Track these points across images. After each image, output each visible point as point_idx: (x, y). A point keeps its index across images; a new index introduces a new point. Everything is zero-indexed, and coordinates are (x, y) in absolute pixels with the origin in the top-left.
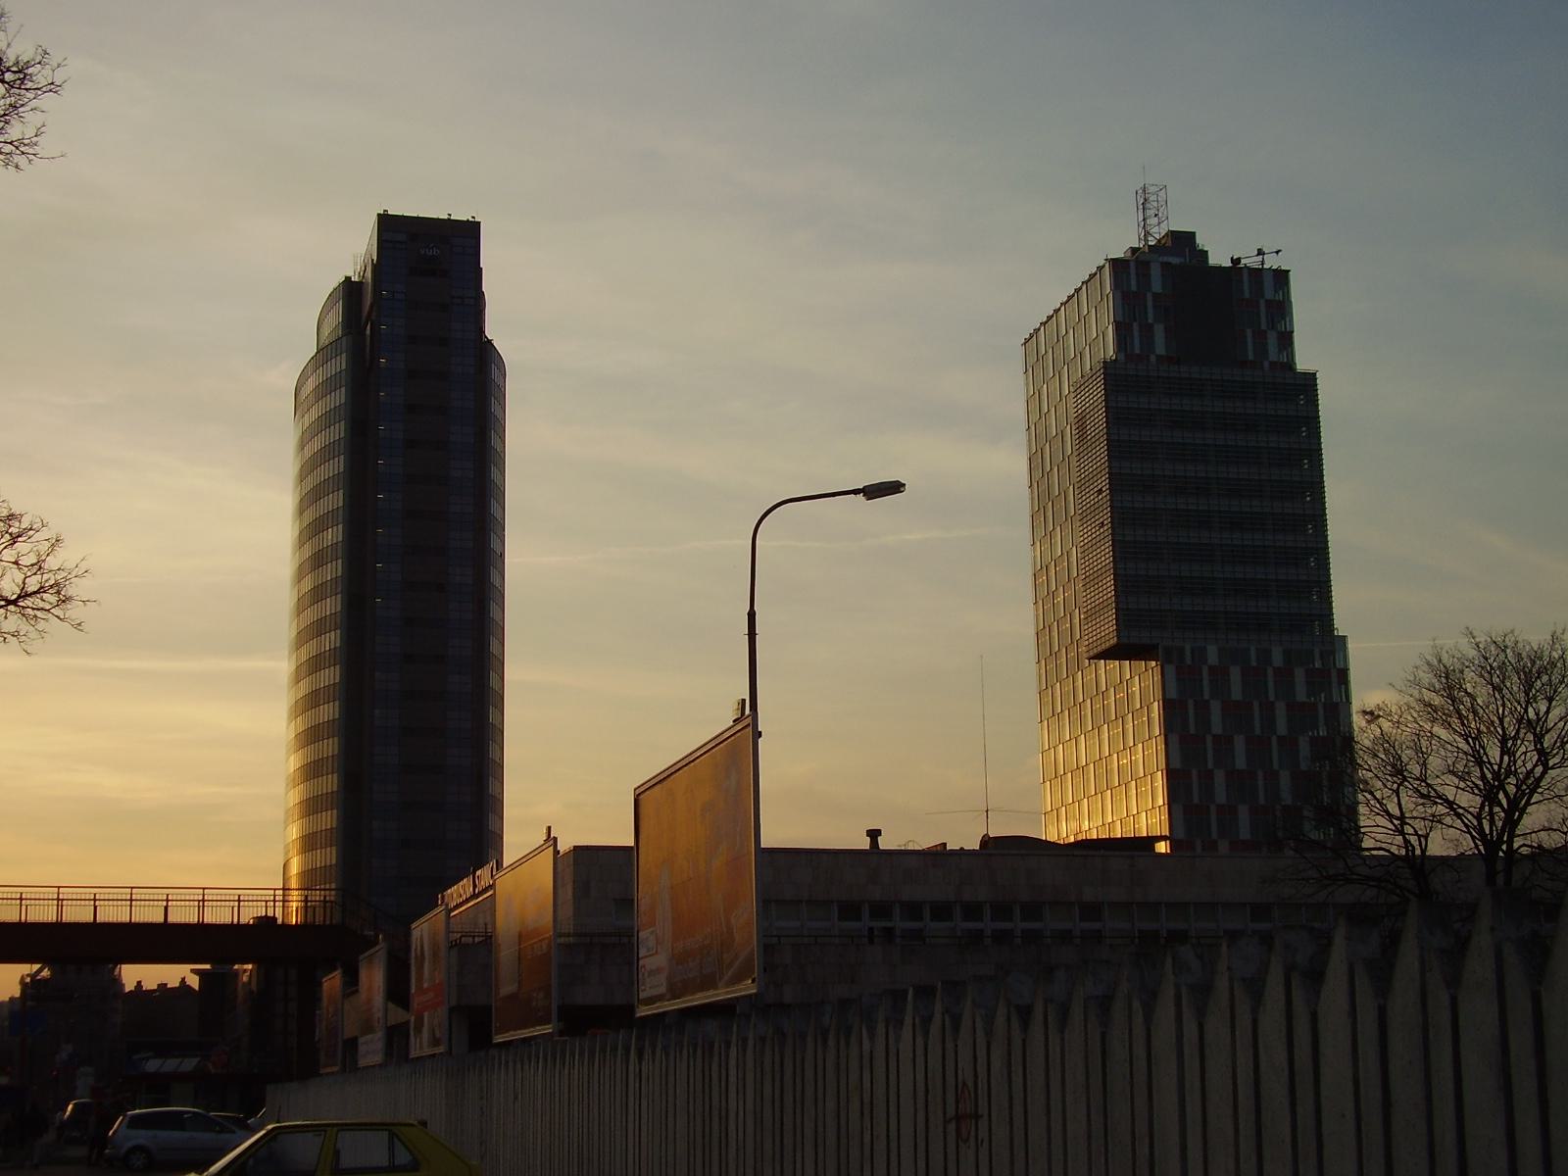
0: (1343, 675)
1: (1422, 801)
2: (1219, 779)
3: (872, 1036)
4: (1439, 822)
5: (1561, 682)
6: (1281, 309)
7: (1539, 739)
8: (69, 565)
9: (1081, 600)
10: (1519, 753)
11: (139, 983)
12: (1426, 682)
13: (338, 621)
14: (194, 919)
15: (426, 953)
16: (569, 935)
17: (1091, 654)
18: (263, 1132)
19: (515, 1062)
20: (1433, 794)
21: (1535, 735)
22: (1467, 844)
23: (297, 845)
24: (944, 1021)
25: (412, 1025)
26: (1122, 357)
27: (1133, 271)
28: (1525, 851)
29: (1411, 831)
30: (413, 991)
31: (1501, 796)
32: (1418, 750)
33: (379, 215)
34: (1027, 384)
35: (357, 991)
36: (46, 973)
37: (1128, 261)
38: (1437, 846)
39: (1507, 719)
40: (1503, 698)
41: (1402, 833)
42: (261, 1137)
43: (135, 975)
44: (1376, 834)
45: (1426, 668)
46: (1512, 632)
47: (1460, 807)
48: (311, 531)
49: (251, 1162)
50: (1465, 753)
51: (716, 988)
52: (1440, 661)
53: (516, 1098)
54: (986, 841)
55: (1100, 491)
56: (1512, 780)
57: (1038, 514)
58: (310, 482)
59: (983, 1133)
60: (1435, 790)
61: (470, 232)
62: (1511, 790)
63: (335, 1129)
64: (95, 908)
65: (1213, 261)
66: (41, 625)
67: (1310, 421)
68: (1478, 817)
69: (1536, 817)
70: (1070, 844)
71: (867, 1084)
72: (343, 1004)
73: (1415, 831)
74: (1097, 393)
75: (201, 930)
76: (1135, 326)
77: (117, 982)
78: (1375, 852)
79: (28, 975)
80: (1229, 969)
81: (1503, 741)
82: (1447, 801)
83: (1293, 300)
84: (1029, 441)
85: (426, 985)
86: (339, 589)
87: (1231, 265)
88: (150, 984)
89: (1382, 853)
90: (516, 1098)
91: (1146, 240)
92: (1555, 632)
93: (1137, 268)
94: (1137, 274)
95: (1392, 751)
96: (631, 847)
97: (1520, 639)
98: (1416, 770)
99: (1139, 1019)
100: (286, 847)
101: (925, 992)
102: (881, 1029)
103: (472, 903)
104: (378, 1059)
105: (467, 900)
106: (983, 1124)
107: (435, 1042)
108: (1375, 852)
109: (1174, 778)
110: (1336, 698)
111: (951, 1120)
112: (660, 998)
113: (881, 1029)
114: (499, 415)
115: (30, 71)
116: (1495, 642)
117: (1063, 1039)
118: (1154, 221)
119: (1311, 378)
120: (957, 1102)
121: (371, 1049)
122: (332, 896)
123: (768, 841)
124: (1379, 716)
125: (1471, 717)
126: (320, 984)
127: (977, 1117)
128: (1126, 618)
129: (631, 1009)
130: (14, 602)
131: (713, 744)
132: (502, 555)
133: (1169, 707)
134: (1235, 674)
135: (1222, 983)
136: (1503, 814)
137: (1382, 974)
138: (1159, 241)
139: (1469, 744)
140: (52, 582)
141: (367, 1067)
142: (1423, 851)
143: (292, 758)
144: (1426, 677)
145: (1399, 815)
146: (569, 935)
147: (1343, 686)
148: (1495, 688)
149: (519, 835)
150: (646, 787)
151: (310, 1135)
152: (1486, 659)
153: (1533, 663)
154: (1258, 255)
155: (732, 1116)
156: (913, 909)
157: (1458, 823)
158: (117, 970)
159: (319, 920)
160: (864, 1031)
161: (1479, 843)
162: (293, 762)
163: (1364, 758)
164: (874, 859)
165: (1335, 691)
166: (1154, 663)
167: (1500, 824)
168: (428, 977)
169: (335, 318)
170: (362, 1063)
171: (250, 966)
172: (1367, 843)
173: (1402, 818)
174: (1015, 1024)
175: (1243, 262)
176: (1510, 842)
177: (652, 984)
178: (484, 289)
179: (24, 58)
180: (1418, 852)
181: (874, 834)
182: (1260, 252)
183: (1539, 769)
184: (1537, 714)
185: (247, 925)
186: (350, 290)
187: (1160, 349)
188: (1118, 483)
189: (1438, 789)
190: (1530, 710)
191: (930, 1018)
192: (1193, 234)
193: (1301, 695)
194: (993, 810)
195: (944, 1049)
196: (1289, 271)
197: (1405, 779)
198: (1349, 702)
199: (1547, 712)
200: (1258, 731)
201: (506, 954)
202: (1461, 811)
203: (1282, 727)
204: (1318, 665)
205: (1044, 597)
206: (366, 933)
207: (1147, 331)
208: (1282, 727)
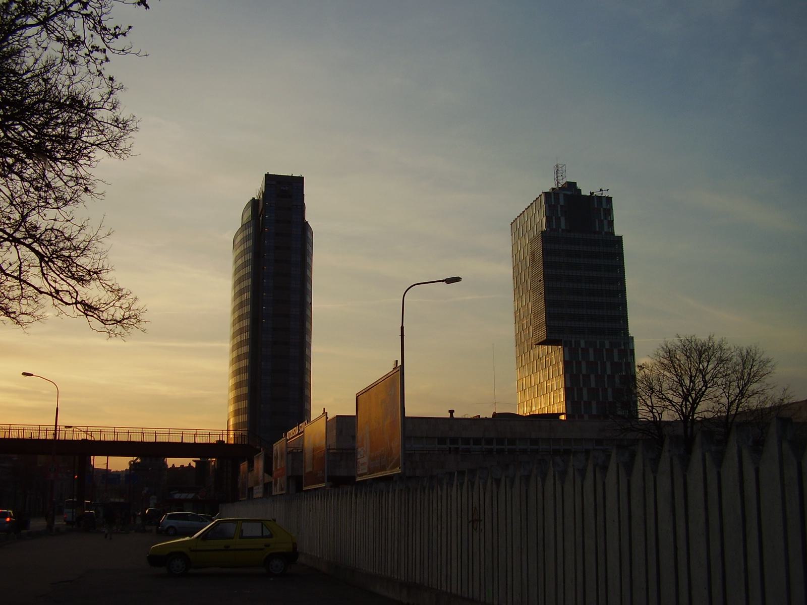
0: (632, 351)
1: (660, 400)
2: (585, 392)
3: (441, 490)
4: (666, 408)
5: (712, 355)
6: (609, 212)
7: (704, 377)
8: (141, 308)
9: (533, 322)
10: (696, 382)
11: (173, 465)
12: (661, 355)
13: (249, 328)
14: (192, 441)
15: (279, 456)
17: (537, 343)
18: (214, 522)
19: (310, 498)
20: (664, 397)
21: (702, 375)
22: (677, 416)
23: (233, 414)
24: (468, 484)
25: (273, 482)
26: (548, 229)
27: (553, 197)
28: (698, 419)
29: (656, 411)
30: (274, 469)
31: (690, 398)
32: (658, 380)
33: (265, 174)
34: (512, 240)
35: (253, 470)
36: (139, 460)
37: (551, 193)
38: (665, 417)
39: (692, 369)
40: (691, 361)
41: (652, 412)
42: (213, 525)
43: (172, 462)
44: (643, 413)
45: (661, 349)
46: (694, 336)
47: (674, 402)
48: (238, 294)
49: (210, 533)
50: (676, 382)
51: (386, 471)
52: (667, 347)
53: (310, 511)
54: (495, 415)
55: (540, 281)
56: (694, 392)
57: (517, 289)
58: (238, 276)
59: (482, 527)
60: (665, 396)
61: (300, 180)
62: (694, 396)
63: (241, 522)
64: (156, 436)
65: (583, 193)
66: (130, 330)
68: (681, 406)
69: (702, 406)
70: (528, 416)
71: (439, 508)
72: (248, 474)
73: (657, 411)
74: (539, 245)
75: (195, 445)
76: (554, 217)
77: (165, 464)
78: (642, 420)
79: (132, 461)
80: (573, 465)
81: (691, 377)
82: (669, 400)
83: (613, 208)
84: (513, 261)
85: (278, 468)
86: (249, 316)
87: (589, 195)
88: (177, 465)
89: (644, 420)
90: (310, 511)
91: (558, 185)
92: (710, 336)
93: (554, 196)
94: (554, 198)
95: (648, 381)
96: (355, 416)
97: (697, 339)
98: (658, 388)
99: (540, 484)
100: (228, 414)
101: (461, 473)
102: (445, 487)
103: (298, 436)
104: (260, 495)
105: (296, 435)
106: (482, 523)
107: (282, 489)
108: (642, 420)
109: (568, 391)
110: (629, 361)
111: (470, 522)
112: (365, 474)
113: (445, 487)
114: (310, 250)
115: (128, 123)
116: (688, 340)
117: (512, 491)
118: (561, 178)
119: (620, 238)
120: (473, 515)
121: (258, 492)
122: (245, 433)
123: (408, 413)
124: (644, 368)
125: (679, 368)
126: (240, 466)
127: (480, 521)
128: (549, 329)
129: (354, 478)
130: (120, 322)
131: (386, 377)
132: (311, 304)
133: (566, 364)
134: (591, 351)
135: (590, 468)
136: (690, 405)
137: (629, 467)
138: (563, 185)
139: (677, 378)
140: (133, 314)
141: (257, 498)
142: (660, 419)
143: (231, 380)
144: (662, 353)
145: (651, 405)
146: (334, 449)
147: (632, 356)
148: (688, 357)
149: (315, 412)
150: (361, 393)
151: (231, 524)
152: (685, 346)
153: (702, 348)
154: (600, 191)
155: (390, 520)
156: (466, 441)
157: (673, 409)
158: (165, 460)
159: (240, 442)
160: (439, 487)
161: (681, 416)
162: (231, 382)
163: (639, 384)
164: (451, 421)
165: (629, 358)
166: (560, 347)
167: (689, 409)
168: (279, 464)
169: (249, 213)
170: (255, 496)
171: (214, 459)
172: (640, 416)
173: (652, 407)
174: (494, 486)
175: (595, 194)
176: (693, 416)
177: (362, 469)
178: (305, 202)
179: (126, 119)
180: (658, 419)
181: (451, 412)
182: (601, 190)
183: (704, 388)
184: (703, 367)
185: (214, 444)
186: (254, 203)
187: (563, 226)
188: (547, 278)
189: (666, 395)
190: (701, 365)
191: (464, 482)
192: (575, 183)
193: (616, 359)
194: (498, 403)
195: (468, 495)
197: (653, 392)
198: (634, 362)
199: (707, 366)
200: (600, 373)
201: (308, 456)
202: (674, 404)
203: (609, 372)
204: (623, 347)
205: (518, 319)
206: (257, 447)
207: (558, 219)
208: (609, 372)
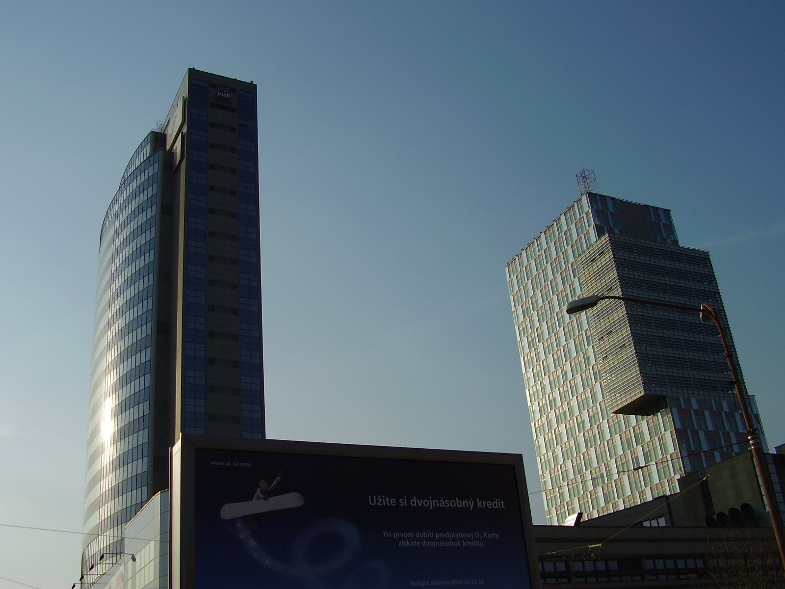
67: (710, 278)
196: (670, 211)
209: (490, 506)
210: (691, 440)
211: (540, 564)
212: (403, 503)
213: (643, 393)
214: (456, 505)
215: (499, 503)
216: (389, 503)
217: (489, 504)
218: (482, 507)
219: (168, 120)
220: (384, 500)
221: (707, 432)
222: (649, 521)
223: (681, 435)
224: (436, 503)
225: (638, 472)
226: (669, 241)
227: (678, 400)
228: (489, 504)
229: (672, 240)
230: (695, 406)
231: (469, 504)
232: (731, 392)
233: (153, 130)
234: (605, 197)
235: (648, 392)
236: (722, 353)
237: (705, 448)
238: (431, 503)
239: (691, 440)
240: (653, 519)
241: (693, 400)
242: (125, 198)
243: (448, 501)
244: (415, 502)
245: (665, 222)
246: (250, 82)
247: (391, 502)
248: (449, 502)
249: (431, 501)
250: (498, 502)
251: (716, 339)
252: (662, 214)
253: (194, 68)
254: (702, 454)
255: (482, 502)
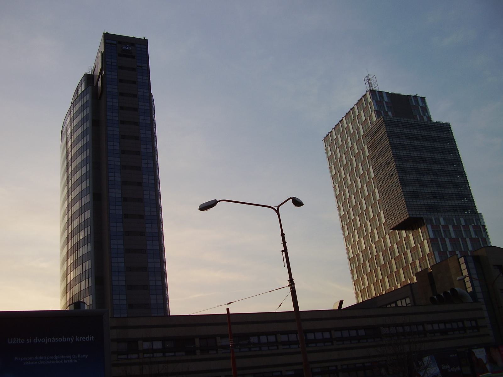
16: (297, 336)
17: (392, 227)
67: (451, 140)
146: (297, 336)
186: (89, 79)
196: (425, 98)
209: (84, 340)
210: (441, 245)
211: (299, 339)
212: (29, 341)
213: (408, 216)
214: (63, 340)
215: (90, 338)
216: (21, 342)
217: (84, 339)
218: (79, 340)
219: (94, 66)
220: (17, 340)
221: (451, 239)
222: (400, 301)
223: (433, 242)
224: (49, 340)
225: (436, 262)
226: (425, 118)
227: (431, 220)
228: (84, 339)
229: (427, 117)
230: (442, 222)
231: (71, 339)
232: (466, 212)
233: (86, 73)
234: (381, 92)
235: (411, 216)
236: (460, 188)
237: (450, 248)
238: (46, 340)
239: (441, 245)
240: (403, 299)
241: (441, 220)
242: (74, 113)
243: (57, 338)
244: (36, 340)
245: (422, 106)
246: (143, 38)
247: (22, 341)
248: (58, 339)
249: (46, 339)
250: (90, 337)
251: (456, 179)
252: (419, 100)
253: (107, 33)
254: (448, 252)
255: (80, 338)
